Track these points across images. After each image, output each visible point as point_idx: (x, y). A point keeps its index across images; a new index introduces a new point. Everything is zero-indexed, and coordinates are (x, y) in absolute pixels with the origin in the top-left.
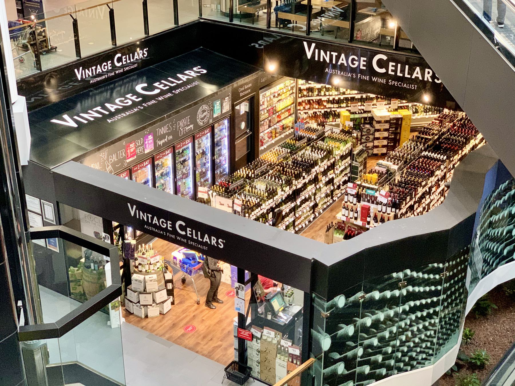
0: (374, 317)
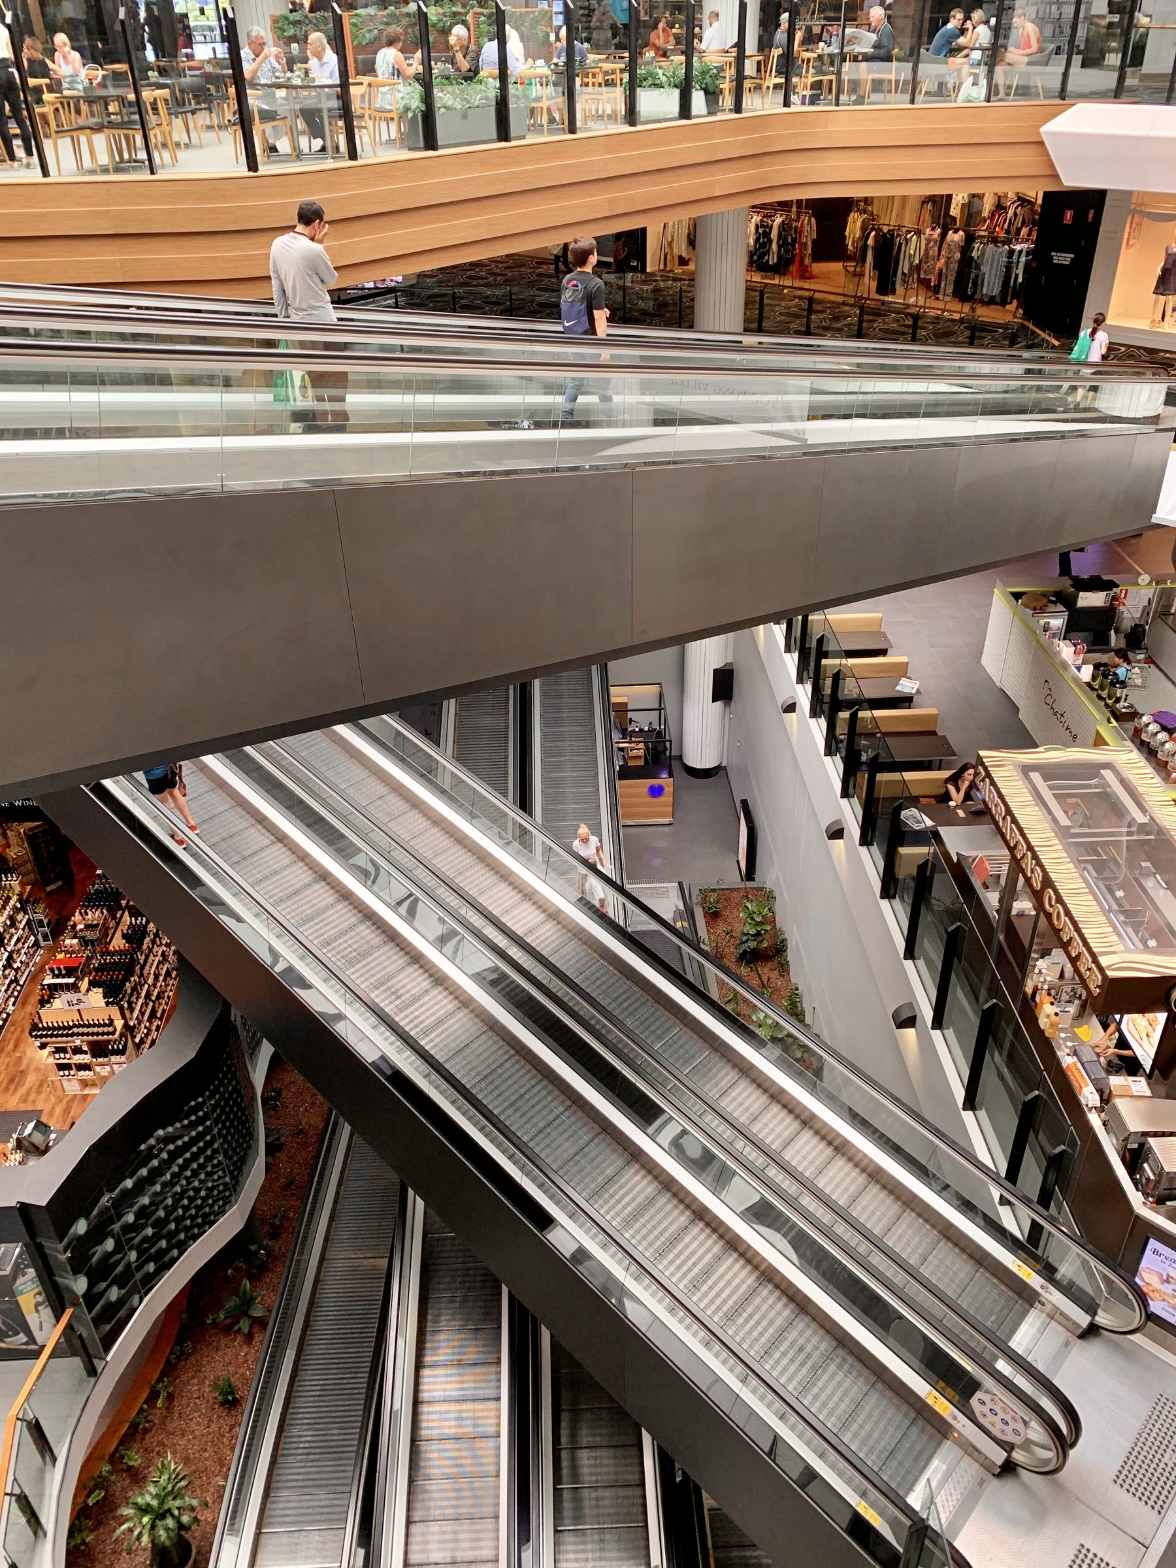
0: (135, 1208)
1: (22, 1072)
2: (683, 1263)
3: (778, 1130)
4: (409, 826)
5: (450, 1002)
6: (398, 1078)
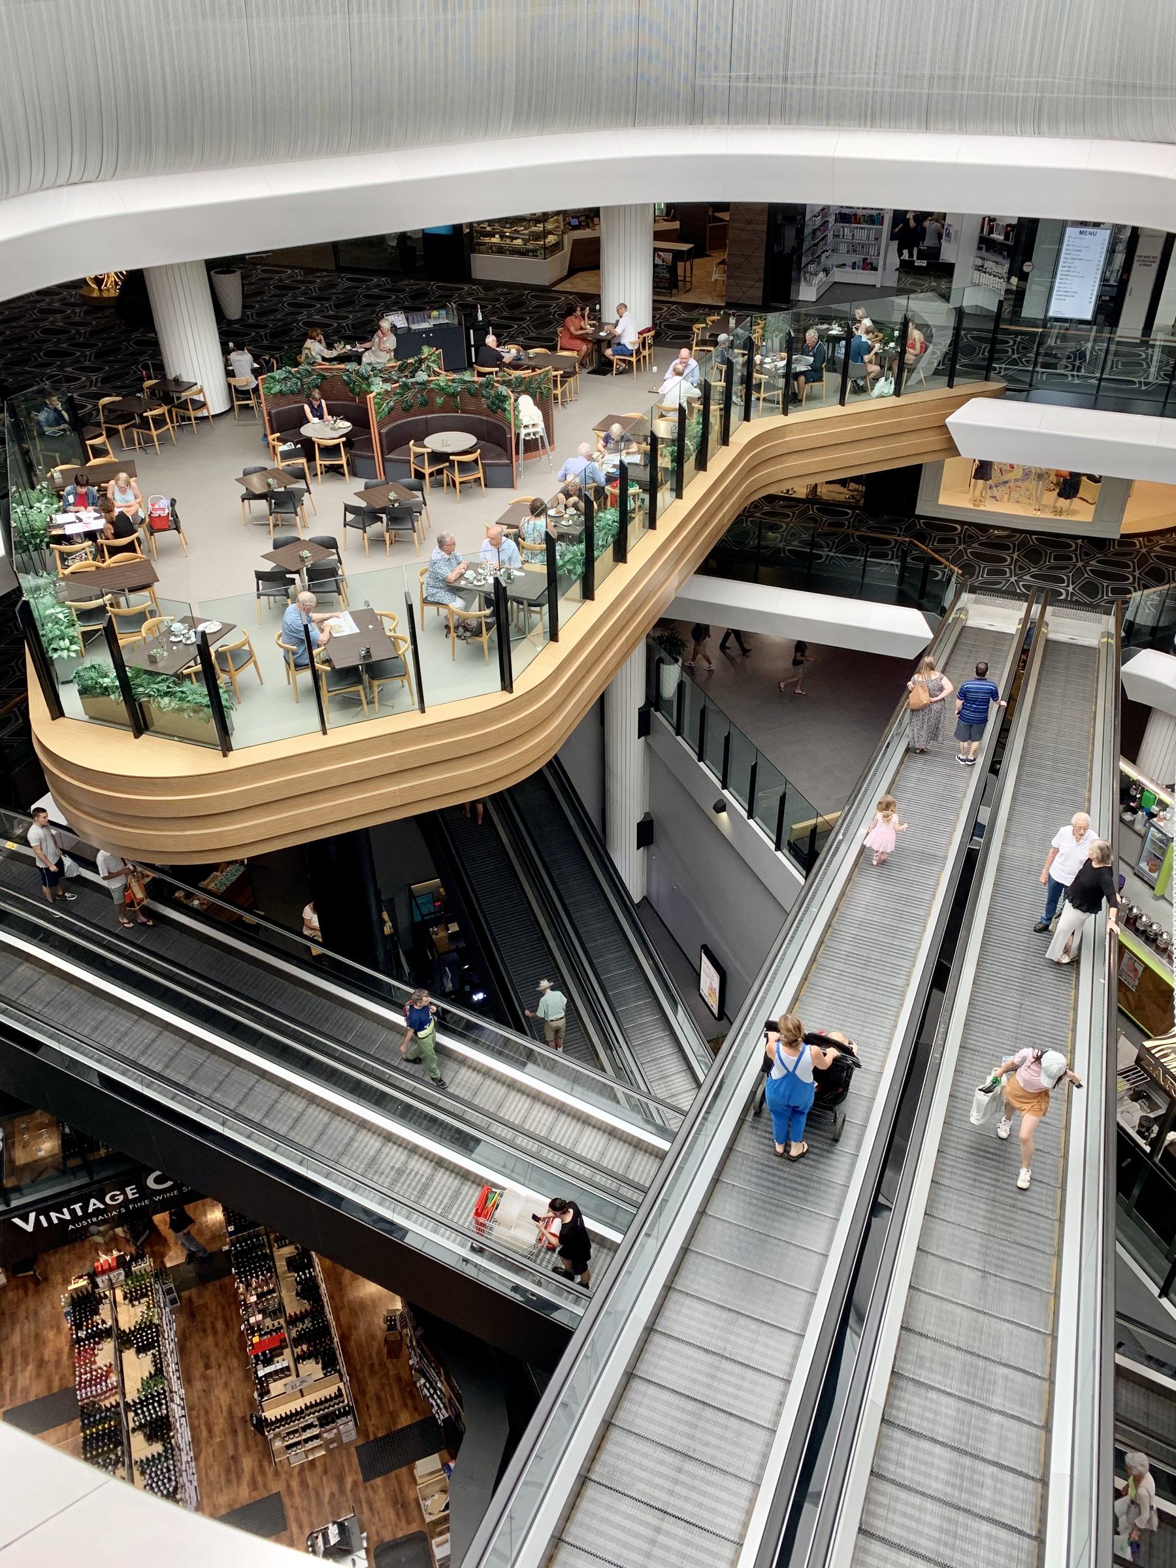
1: (233, 1457)
2: (463, 1212)
4: (515, 1109)
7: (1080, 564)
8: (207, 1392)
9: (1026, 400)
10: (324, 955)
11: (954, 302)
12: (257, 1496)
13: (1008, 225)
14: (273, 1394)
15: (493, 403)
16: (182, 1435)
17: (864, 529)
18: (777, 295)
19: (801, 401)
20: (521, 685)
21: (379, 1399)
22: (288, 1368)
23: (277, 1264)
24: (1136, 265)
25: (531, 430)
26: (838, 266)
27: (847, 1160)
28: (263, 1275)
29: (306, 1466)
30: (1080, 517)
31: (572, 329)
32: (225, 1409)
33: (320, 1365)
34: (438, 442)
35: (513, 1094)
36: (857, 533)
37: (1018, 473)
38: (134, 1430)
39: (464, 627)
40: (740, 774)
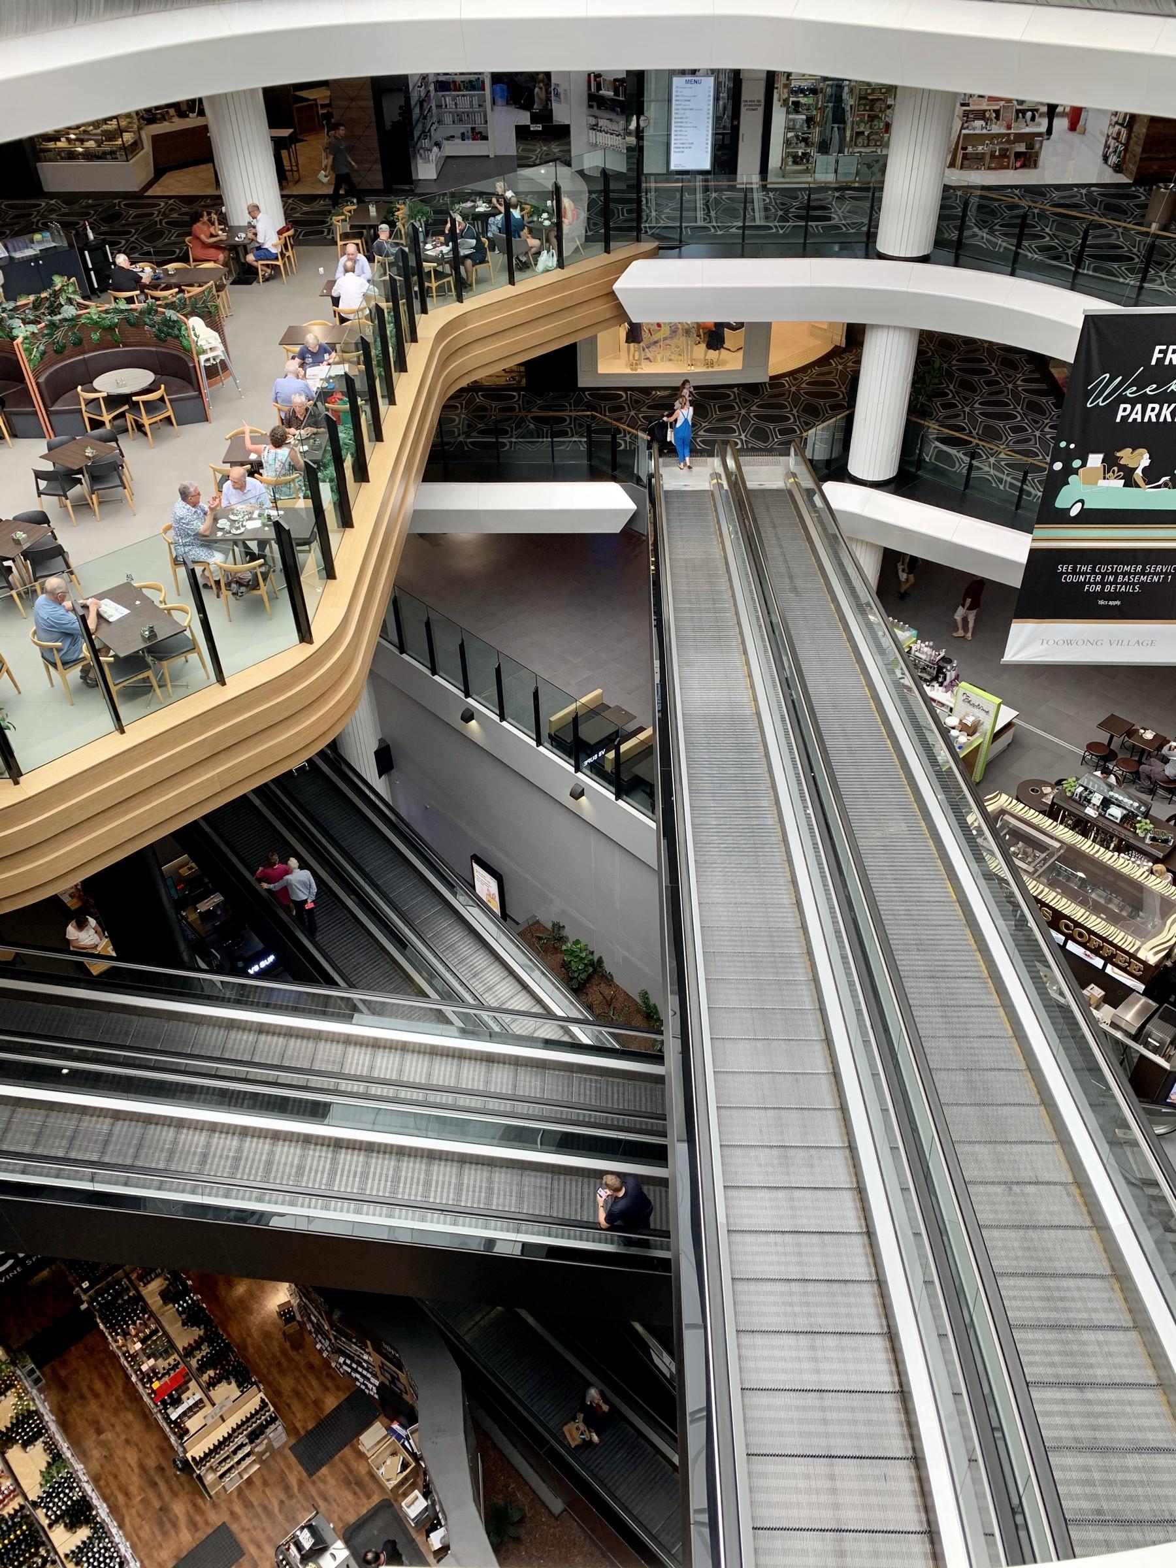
1: (161, 1509)
3: (390, 1066)
5: (264, 1143)
6: (553, 1251)
7: (743, 412)
8: (108, 1458)
9: (680, 257)
10: (113, 967)
11: (576, 166)
12: (201, 1535)
13: (616, 80)
14: (192, 1432)
15: (159, 330)
16: (102, 1511)
17: (535, 409)
18: (398, 177)
19: (471, 285)
20: (321, 629)
21: (297, 1394)
22: (201, 1401)
23: (149, 1302)
24: (743, 109)
25: (210, 355)
26: (448, 139)
27: (439, 1032)
28: (139, 1318)
29: (243, 1486)
30: (729, 365)
31: (203, 237)
32: (135, 1466)
33: (234, 1384)
34: (109, 383)
35: (351, 1049)
36: (531, 415)
37: (665, 331)
38: (50, 1526)
39: (237, 582)
40: (482, 674)
